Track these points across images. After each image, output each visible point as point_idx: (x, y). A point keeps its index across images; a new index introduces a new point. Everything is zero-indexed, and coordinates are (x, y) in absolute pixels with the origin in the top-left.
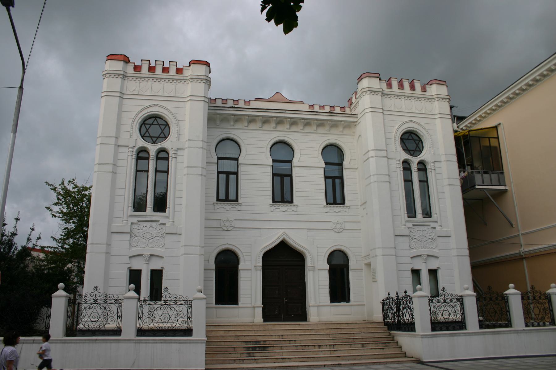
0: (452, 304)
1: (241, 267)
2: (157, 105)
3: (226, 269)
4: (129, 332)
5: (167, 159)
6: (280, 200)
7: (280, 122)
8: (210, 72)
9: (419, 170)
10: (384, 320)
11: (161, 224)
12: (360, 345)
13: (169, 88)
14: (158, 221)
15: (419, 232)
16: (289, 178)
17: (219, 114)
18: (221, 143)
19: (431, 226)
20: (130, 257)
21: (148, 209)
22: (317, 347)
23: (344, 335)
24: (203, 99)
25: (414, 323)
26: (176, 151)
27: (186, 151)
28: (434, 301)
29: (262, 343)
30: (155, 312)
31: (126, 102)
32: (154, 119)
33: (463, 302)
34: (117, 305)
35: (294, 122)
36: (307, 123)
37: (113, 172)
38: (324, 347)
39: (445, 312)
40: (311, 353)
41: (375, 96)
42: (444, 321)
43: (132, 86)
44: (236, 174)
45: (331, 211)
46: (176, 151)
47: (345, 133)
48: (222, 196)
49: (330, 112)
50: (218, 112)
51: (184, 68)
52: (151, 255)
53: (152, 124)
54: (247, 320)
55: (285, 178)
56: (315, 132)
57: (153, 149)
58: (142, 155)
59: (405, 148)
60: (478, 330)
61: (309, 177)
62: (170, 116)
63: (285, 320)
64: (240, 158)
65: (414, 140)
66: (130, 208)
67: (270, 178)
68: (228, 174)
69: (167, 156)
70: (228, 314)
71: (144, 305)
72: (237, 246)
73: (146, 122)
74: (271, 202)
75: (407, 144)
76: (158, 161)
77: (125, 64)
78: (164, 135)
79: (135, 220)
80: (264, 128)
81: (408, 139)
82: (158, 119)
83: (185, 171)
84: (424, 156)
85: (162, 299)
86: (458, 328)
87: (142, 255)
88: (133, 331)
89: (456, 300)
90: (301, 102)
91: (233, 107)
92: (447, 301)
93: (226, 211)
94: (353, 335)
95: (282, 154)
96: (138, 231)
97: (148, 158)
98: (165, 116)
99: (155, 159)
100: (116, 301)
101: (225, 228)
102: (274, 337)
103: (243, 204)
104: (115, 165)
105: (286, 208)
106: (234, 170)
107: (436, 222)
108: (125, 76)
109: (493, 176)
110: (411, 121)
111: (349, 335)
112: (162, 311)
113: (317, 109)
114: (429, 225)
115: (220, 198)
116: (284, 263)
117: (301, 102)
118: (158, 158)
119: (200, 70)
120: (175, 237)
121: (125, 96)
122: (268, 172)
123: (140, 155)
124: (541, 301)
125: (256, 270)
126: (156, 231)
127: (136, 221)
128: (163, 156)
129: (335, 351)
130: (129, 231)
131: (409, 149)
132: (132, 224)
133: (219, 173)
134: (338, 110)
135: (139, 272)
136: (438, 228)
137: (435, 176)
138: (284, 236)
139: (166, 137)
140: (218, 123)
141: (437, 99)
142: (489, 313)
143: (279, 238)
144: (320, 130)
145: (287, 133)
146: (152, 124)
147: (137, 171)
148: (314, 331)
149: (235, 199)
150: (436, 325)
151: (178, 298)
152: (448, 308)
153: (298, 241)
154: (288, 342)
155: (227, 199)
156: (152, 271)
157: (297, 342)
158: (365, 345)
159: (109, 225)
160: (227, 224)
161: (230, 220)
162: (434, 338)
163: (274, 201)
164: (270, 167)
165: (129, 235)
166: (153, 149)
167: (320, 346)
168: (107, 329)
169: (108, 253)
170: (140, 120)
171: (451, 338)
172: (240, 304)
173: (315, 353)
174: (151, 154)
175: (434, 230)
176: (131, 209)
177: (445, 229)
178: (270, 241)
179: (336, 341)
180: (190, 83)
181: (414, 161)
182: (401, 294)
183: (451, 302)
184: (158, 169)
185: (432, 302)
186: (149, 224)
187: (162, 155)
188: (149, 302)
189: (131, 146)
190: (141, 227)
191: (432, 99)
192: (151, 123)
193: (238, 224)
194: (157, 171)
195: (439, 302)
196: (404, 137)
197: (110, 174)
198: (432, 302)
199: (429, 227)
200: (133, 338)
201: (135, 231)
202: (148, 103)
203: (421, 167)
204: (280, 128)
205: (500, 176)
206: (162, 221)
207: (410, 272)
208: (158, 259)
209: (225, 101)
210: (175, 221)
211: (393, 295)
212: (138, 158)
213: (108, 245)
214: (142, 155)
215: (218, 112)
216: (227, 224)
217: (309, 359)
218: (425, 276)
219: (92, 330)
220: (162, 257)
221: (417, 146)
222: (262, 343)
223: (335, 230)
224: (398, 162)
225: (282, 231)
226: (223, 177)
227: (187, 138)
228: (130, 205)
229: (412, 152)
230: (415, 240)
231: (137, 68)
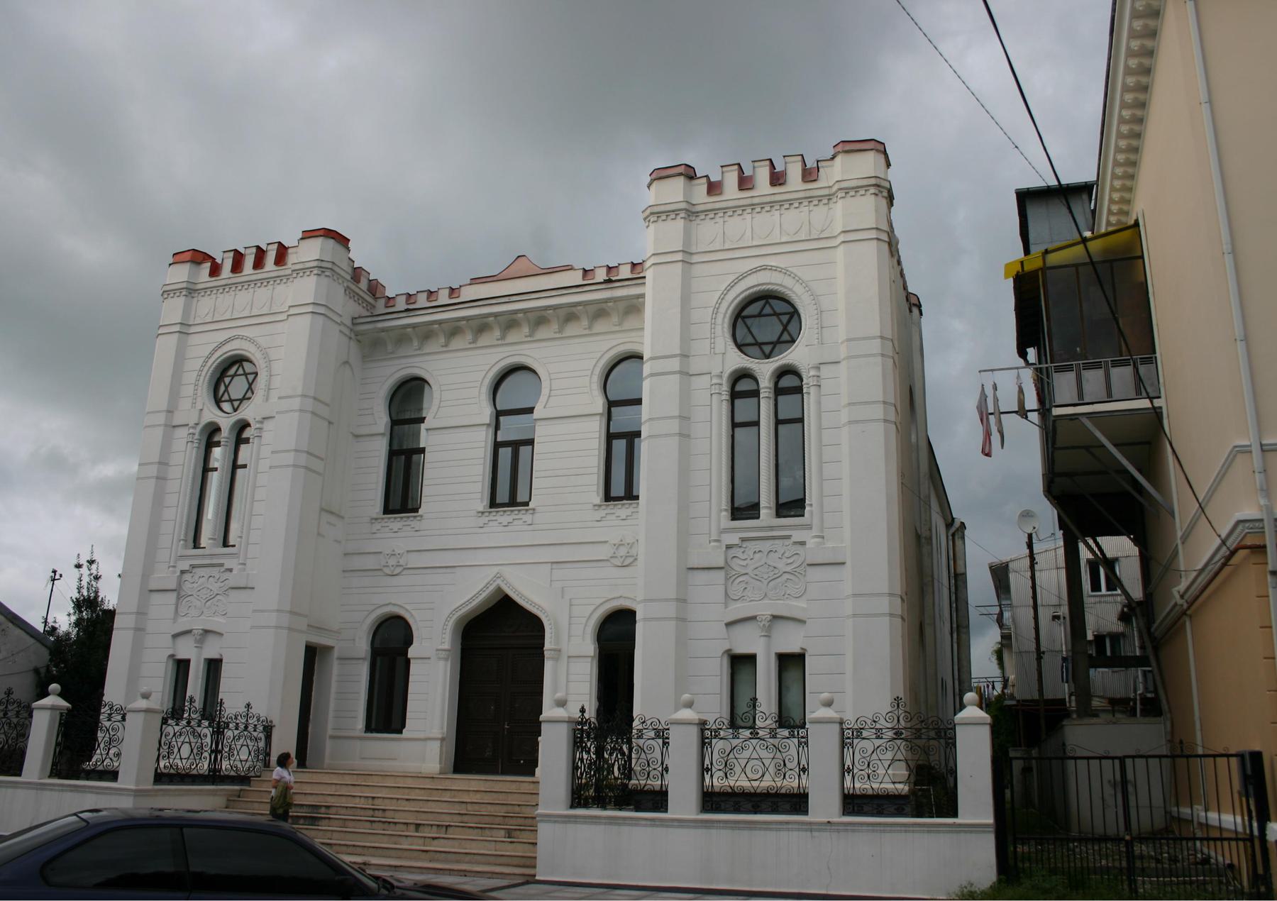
0: (775, 741)
1: (412, 652)
4: (683, 799)
5: (799, 390)
6: (398, 507)
7: (510, 323)
8: (888, 165)
11: (795, 543)
12: (502, 832)
13: (791, 221)
14: (222, 565)
15: (757, 555)
17: (383, 330)
19: (793, 539)
20: (729, 625)
21: (763, 512)
22: (412, 827)
23: (497, 808)
24: (873, 234)
25: (666, 792)
26: (261, 422)
27: (844, 363)
29: (323, 810)
30: (874, 756)
31: (697, 270)
32: (763, 302)
35: (539, 319)
36: (570, 315)
37: (680, 435)
38: (427, 829)
39: (751, 763)
40: (386, 838)
41: (670, 223)
43: (708, 232)
45: (609, 517)
46: (818, 368)
47: (480, 343)
48: (503, 496)
49: (609, 281)
50: (380, 325)
52: (775, 617)
54: (412, 766)
55: (522, 449)
56: (558, 335)
57: (765, 370)
60: (150, 787)
62: (798, 289)
63: (504, 773)
66: (724, 513)
68: (516, 445)
69: (754, 387)
70: (384, 749)
72: (408, 607)
75: (754, 330)
76: (780, 398)
77: (193, 266)
78: (787, 338)
79: (733, 539)
80: (480, 343)
81: (760, 315)
82: (773, 302)
83: (844, 416)
84: (795, 355)
86: (749, 806)
87: (753, 618)
88: (836, 802)
89: (652, 734)
90: (569, 268)
91: (407, 310)
93: (526, 527)
94: (517, 809)
96: (744, 563)
97: (755, 394)
98: (776, 288)
99: (772, 395)
101: (387, 571)
102: (357, 800)
103: (425, 516)
105: (510, 519)
108: (691, 213)
109: (1116, 372)
111: (510, 808)
113: (444, 298)
114: (788, 537)
116: (501, 640)
117: (569, 268)
118: (779, 391)
119: (866, 164)
120: (242, 595)
121: (695, 259)
123: (739, 388)
124: (199, 729)
126: (785, 560)
127: (737, 541)
128: (789, 383)
129: (434, 838)
130: (721, 564)
131: (775, 339)
132: (729, 547)
134: (422, 301)
135: (751, 659)
136: (811, 542)
137: (819, 403)
138: (499, 582)
139: (793, 341)
140: (390, 348)
141: (841, 194)
143: (486, 587)
144: (600, 326)
145: (526, 346)
146: (227, 387)
147: (734, 425)
148: (448, 793)
154: (371, 813)
157: (388, 814)
158: (514, 834)
159: (682, 550)
160: (392, 562)
161: (397, 551)
162: (569, 825)
165: (174, 595)
166: (765, 370)
167: (418, 826)
169: (681, 620)
170: (730, 312)
171: (615, 828)
172: (406, 733)
173: (394, 839)
174: (762, 385)
175: (799, 549)
176: (726, 515)
177: (829, 545)
178: (467, 593)
179: (466, 818)
180: (840, 202)
184: (780, 417)
186: (767, 546)
187: (787, 382)
189: (191, 424)
190: (196, 577)
191: (829, 197)
193: (415, 560)
194: (778, 422)
195: (878, 737)
197: (674, 442)
199: (787, 542)
200: (150, 787)
201: (735, 564)
204: (513, 336)
205: (1142, 369)
206: (797, 535)
208: (791, 625)
210: (248, 562)
212: (734, 395)
213: (682, 601)
214: (743, 386)
215: (380, 325)
217: (365, 851)
218: (766, 672)
219: (178, 775)
220: (802, 622)
222: (323, 810)
224: (715, 381)
225: (496, 569)
227: (841, 334)
228: (724, 507)
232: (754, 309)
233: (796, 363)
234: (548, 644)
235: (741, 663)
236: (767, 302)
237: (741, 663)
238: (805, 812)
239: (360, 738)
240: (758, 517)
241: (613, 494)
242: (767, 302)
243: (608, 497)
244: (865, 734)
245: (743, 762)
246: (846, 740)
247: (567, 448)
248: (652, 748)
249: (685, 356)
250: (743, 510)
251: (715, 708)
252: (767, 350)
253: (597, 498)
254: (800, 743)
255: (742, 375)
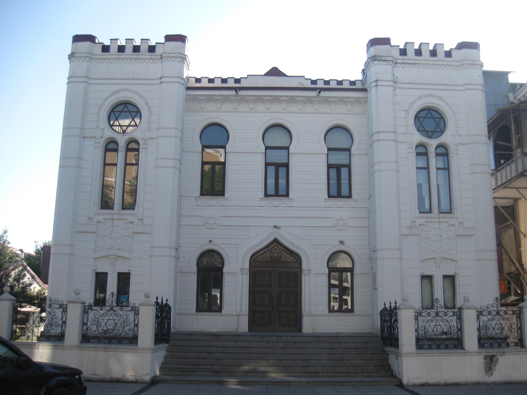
0: (446, 318)
1: (225, 270)
2: (126, 90)
3: (210, 272)
5: (137, 150)
6: (274, 193)
9: (437, 155)
10: (381, 335)
16: (347, 169)
18: (330, 132)
28: (423, 314)
33: (460, 315)
34: (61, 310)
42: (435, 337)
44: (349, 166)
51: (157, 45)
53: (122, 111)
58: (422, 151)
59: (421, 128)
61: (308, 170)
64: (290, 147)
65: (434, 118)
67: (262, 167)
68: (278, 166)
71: (89, 311)
72: (222, 246)
73: (115, 110)
74: (326, 197)
76: (108, 153)
84: (447, 138)
85: (107, 304)
89: (511, 313)
92: (440, 314)
95: (277, 139)
97: (116, 150)
100: (61, 306)
104: (80, 159)
106: (284, 161)
107: (457, 218)
110: (430, 95)
112: (107, 318)
115: (331, 194)
118: (128, 150)
122: (260, 161)
123: (131, 146)
125: (243, 274)
128: (444, 152)
132: (98, 222)
133: (267, 164)
142: (494, 329)
146: (122, 111)
147: (105, 164)
149: (348, 194)
150: (424, 342)
151: (53, 301)
152: (441, 323)
153: (291, 239)
155: (277, 194)
156: (120, 274)
163: (330, 196)
164: (261, 155)
168: (52, 334)
178: (258, 240)
181: (432, 143)
182: (393, 305)
183: (446, 315)
184: (107, 162)
185: (421, 315)
187: (133, 145)
188: (94, 308)
192: (121, 110)
194: (126, 164)
195: (490, 315)
196: (420, 115)
198: (421, 315)
202: (116, 88)
203: (441, 150)
206: (130, 218)
207: (419, 279)
209: (327, 82)
211: (388, 306)
212: (107, 150)
216: (211, 221)
221: (438, 125)
223: (337, 227)
224: (410, 146)
226: (333, 172)
229: (430, 134)
230: (428, 240)
231: (106, 49)
232: (120, 108)
233: (136, 137)
234: (304, 267)
235: (427, 279)
236: (126, 106)
237: (427, 279)
238: (136, 343)
239: (194, 315)
240: (134, 209)
241: (268, 193)
242: (126, 106)
243: (266, 195)
244: (484, 313)
245: (106, 321)
246: (480, 313)
247: (308, 170)
248: (452, 320)
249: (82, 128)
250: (106, 204)
251: (89, 297)
252: (430, 134)
253: (262, 195)
254: (63, 311)
255: (420, 145)
